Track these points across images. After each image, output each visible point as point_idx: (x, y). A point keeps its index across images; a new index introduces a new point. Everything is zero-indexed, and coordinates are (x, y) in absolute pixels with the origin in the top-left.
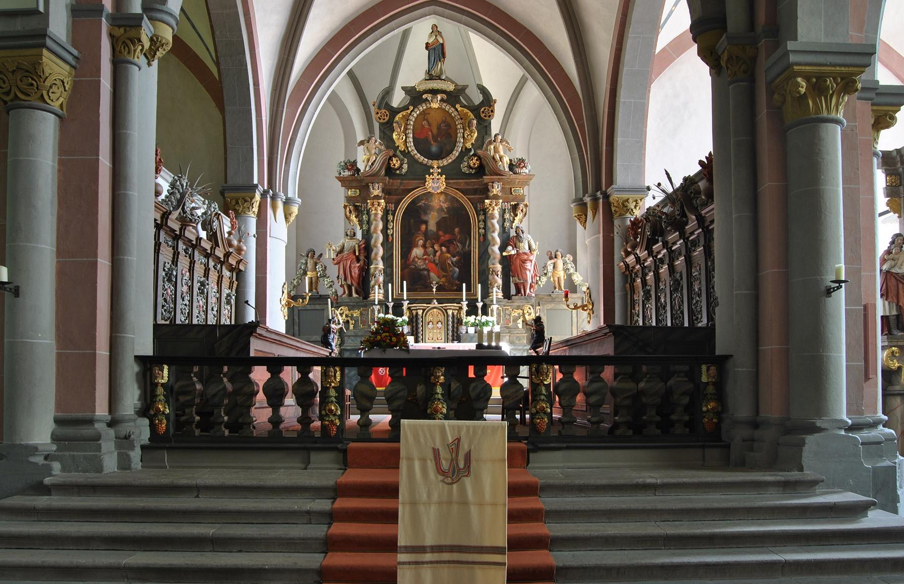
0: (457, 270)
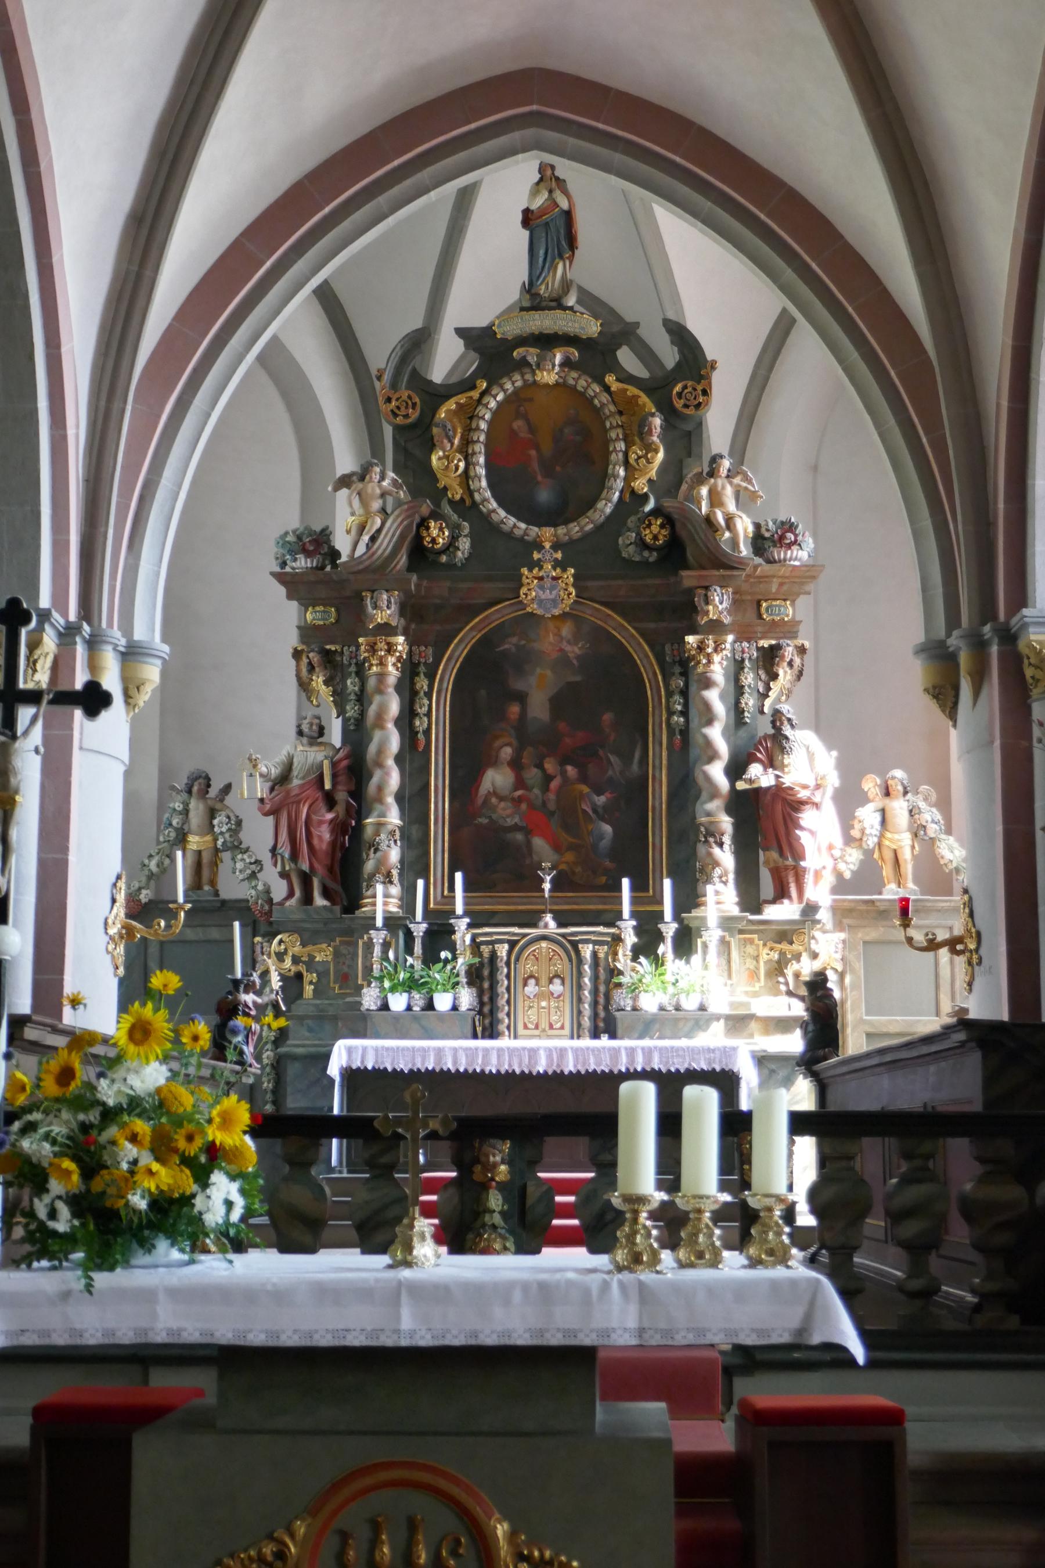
0: (608, 829)
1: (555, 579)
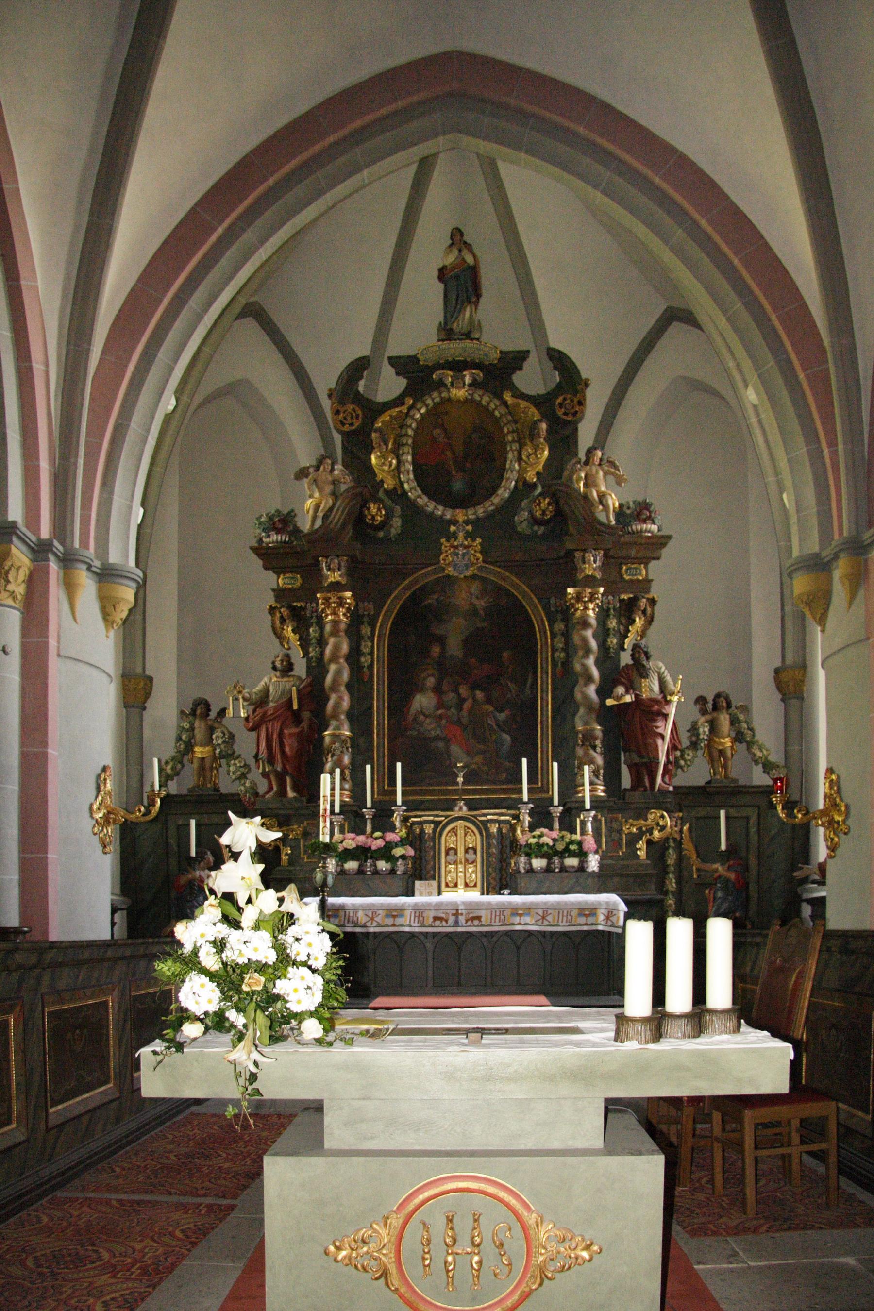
0: (507, 737)
1: (466, 547)
